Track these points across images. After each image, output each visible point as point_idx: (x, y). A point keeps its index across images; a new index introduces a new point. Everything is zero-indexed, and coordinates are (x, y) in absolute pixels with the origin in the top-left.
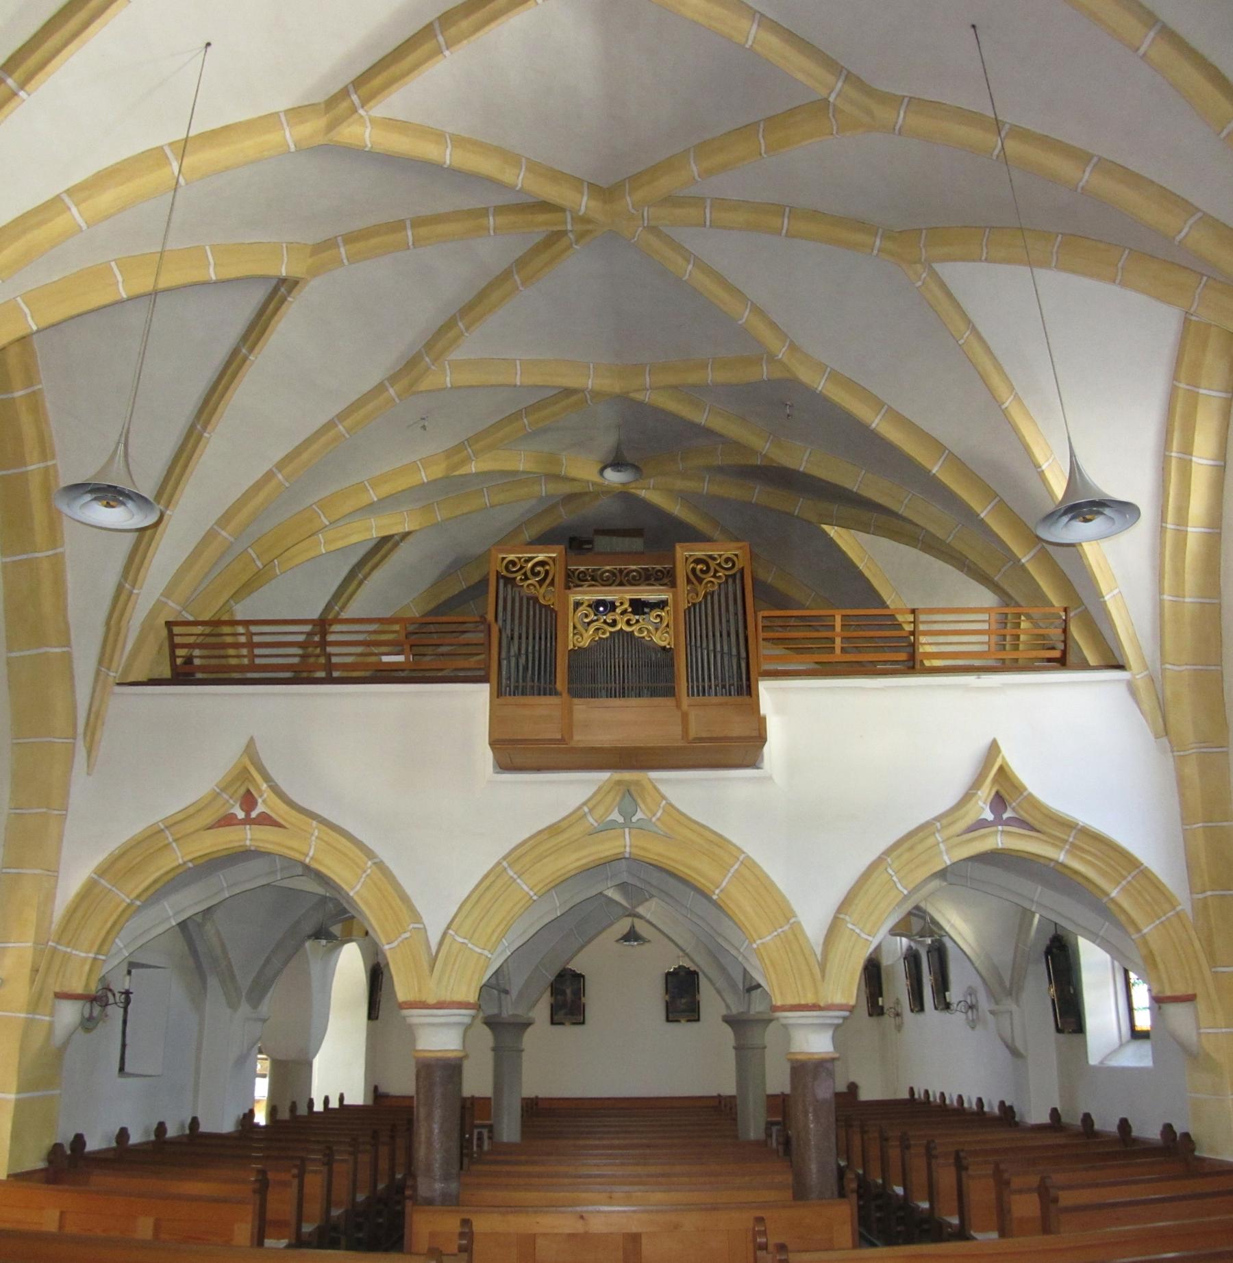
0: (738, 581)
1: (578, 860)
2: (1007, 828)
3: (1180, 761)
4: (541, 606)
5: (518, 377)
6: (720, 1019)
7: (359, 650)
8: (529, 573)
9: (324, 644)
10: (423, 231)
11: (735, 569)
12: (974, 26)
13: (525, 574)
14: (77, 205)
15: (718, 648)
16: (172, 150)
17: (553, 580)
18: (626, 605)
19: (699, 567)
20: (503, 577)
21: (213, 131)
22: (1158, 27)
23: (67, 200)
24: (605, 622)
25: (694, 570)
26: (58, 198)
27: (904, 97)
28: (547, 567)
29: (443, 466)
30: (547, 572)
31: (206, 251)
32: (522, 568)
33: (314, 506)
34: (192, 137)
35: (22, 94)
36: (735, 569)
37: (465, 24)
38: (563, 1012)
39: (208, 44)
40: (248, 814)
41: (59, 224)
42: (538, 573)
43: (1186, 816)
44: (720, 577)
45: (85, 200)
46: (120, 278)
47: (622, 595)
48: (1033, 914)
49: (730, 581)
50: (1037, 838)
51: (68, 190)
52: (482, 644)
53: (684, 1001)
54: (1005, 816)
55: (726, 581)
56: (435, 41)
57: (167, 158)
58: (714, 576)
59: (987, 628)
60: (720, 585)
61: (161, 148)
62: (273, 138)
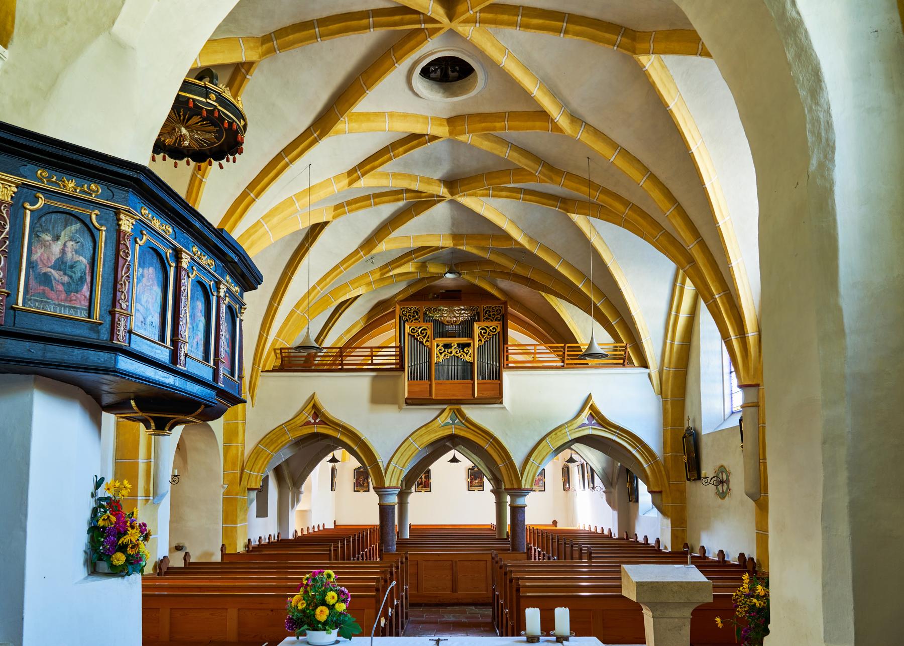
0: (497, 336)
1: (435, 436)
2: (593, 427)
3: (665, 403)
4: (425, 346)
5: (412, 244)
7: (353, 354)
8: (420, 333)
9: (341, 356)
10: (376, 200)
11: (496, 332)
12: (588, 158)
13: (418, 333)
14: (266, 224)
15: (489, 362)
17: (429, 336)
18: (456, 345)
19: (483, 331)
20: (410, 335)
24: (448, 352)
25: (481, 332)
27: (565, 172)
28: (426, 331)
29: (379, 274)
30: (426, 333)
32: (417, 331)
33: (328, 294)
35: (257, 200)
36: (496, 332)
37: (401, 149)
38: (421, 486)
40: (315, 421)
41: (261, 231)
42: (423, 333)
43: (665, 424)
44: (490, 335)
45: (269, 221)
46: (271, 235)
47: (454, 341)
49: (494, 336)
50: (605, 431)
53: (477, 481)
54: (593, 422)
55: (493, 336)
56: (368, 20)
58: (488, 335)
59: (372, 518)
60: (490, 338)
62: (330, 190)
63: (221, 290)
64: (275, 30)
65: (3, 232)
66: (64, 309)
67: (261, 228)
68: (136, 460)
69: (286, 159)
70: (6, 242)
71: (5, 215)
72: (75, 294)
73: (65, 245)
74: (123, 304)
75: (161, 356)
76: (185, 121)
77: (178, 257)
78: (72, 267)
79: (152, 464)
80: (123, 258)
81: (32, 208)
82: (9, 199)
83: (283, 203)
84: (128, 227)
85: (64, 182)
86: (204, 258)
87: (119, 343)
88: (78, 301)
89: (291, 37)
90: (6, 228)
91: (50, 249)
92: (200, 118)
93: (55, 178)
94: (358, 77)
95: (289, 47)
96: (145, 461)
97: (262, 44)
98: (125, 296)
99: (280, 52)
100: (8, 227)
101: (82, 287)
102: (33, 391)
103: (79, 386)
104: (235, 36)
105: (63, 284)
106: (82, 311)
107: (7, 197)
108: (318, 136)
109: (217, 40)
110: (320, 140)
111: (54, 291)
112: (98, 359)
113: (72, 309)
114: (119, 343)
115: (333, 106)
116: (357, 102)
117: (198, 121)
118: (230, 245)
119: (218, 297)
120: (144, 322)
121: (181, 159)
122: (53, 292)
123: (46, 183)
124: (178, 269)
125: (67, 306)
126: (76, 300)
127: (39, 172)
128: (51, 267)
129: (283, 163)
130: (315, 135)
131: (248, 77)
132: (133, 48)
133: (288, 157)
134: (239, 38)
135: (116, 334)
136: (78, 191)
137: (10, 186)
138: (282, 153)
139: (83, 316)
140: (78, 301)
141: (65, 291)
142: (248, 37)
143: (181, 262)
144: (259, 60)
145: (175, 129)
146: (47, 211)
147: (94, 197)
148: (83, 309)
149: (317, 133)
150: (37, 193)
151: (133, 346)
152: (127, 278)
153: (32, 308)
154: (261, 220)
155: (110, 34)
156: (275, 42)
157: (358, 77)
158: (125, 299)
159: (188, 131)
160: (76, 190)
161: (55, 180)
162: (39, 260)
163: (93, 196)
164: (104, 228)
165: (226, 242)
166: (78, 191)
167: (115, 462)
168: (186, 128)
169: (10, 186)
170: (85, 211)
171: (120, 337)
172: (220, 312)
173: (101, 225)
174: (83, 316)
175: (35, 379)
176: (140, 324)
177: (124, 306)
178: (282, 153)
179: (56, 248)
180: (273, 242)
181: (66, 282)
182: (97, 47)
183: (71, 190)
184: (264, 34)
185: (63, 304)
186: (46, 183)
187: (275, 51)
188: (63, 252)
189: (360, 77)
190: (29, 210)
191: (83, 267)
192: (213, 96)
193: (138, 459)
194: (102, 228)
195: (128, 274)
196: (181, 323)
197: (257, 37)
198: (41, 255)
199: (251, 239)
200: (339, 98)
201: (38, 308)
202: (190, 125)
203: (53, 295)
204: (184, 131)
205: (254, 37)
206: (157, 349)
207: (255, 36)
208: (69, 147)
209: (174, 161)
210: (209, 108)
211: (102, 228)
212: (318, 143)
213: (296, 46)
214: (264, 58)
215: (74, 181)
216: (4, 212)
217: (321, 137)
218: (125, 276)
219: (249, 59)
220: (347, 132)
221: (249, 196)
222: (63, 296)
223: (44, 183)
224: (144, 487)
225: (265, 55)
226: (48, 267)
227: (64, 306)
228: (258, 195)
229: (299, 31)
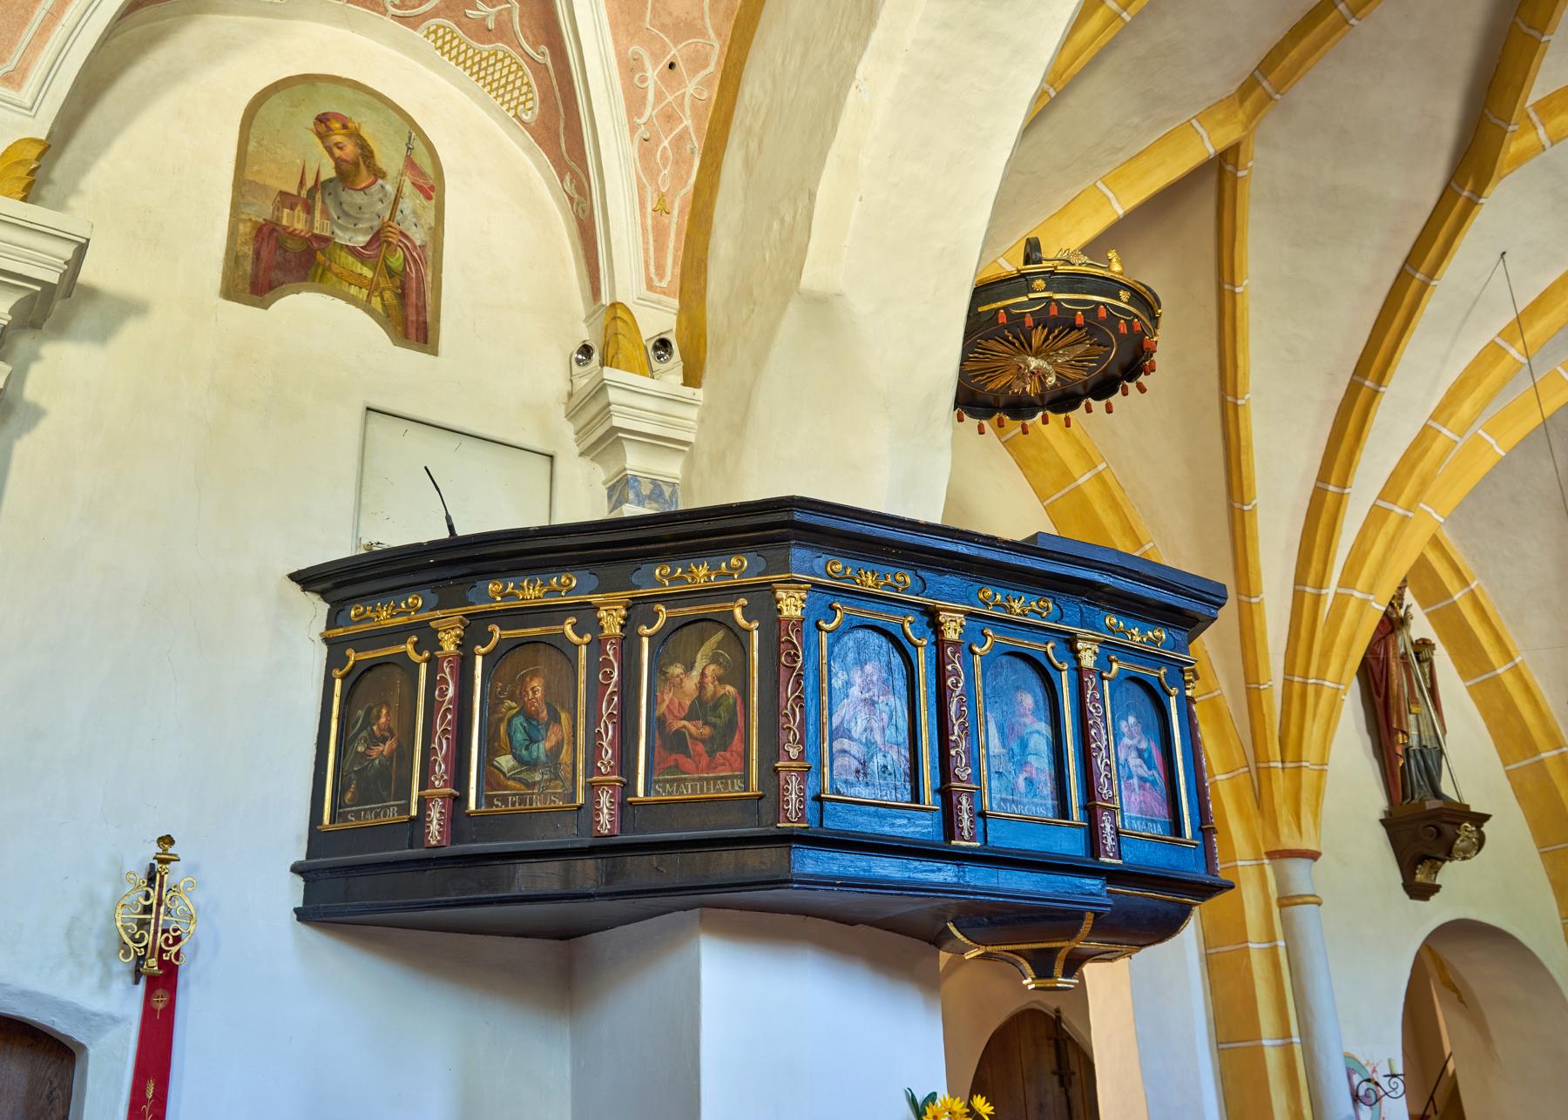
6: (242, 314)
14: (1444, 426)
16: (1503, 339)
21: (1533, 304)
22: (1272, 944)
23: (1434, 425)
26: (1426, 427)
31: (1558, 372)
34: (1550, 417)
35: (1382, 389)
39: (1504, 253)
41: (1437, 447)
45: (1449, 419)
46: (1493, 442)
48: (731, 613)
51: (1431, 416)
52: (821, 825)
57: (1503, 349)
61: (1493, 341)
63: (1082, 654)
64: (1258, 63)
65: (609, 684)
66: (707, 785)
67: (1434, 439)
68: (1256, 1042)
69: (1418, 276)
70: (613, 699)
71: (612, 658)
72: (722, 753)
73: (703, 675)
74: (791, 750)
75: (912, 829)
76: (1026, 345)
77: (931, 617)
78: (715, 707)
79: (1298, 1049)
80: (786, 666)
81: (649, 631)
82: (618, 631)
83: (1478, 361)
84: (794, 608)
85: (691, 572)
86: (1016, 606)
87: (789, 825)
88: (727, 764)
89: (1294, 54)
90: (612, 678)
91: (682, 687)
92: (1044, 328)
93: (680, 570)
94: (1514, 23)
95: (1295, 74)
96: (1279, 1042)
97: (1242, 101)
98: (795, 734)
99: (1282, 94)
100: (616, 674)
101: (732, 738)
102: (699, 942)
103: (803, 914)
104: (1178, 124)
105: (703, 741)
106: (735, 781)
107: (615, 628)
108: (1472, 192)
109: (1144, 150)
110: (1480, 197)
111: (690, 757)
112: (761, 862)
113: (719, 782)
114: (789, 825)
115: (1483, 112)
116: (1531, 74)
117: (1043, 336)
118: (1068, 558)
119: (1079, 671)
120: (863, 770)
121: (1075, 406)
122: (689, 760)
123: (667, 584)
124: (940, 644)
125: (712, 778)
126: (724, 764)
127: (657, 572)
128: (684, 719)
129: (1414, 285)
130: (1466, 193)
131: (1240, 174)
132: (838, 295)
133: (1421, 270)
134: (1189, 121)
135: (784, 809)
136: (712, 578)
137: (616, 610)
138: (1407, 267)
139: (737, 788)
140: (727, 764)
141: (707, 752)
142: (1209, 108)
143: (942, 632)
144: (1245, 133)
145: (1021, 367)
146: (677, 627)
147: (669, 586)
148: (736, 777)
149: (1469, 186)
150: (654, 607)
151: (827, 823)
152: (798, 700)
153: (662, 796)
154: (1430, 423)
155: (799, 293)
156: (1265, 84)
157: (1514, 23)
158: (794, 741)
159: (1042, 358)
160: (709, 577)
161: (681, 573)
162: (666, 713)
163: (736, 576)
164: (755, 625)
165: (1055, 555)
166: (712, 578)
167: (1218, 1050)
168: (1036, 355)
169: (616, 610)
170: (724, 607)
171: (791, 813)
172: (1085, 700)
173: (749, 621)
174: (737, 788)
175: (701, 916)
176: (852, 778)
177: (794, 753)
178: (1407, 267)
179: (691, 683)
180: (1503, 454)
181: (707, 737)
182: (791, 321)
183: (702, 581)
184: (1239, 84)
185: (706, 775)
186: (667, 584)
187: (1271, 98)
188: (701, 686)
189: (1518, 19)
190: (646, 636)
191: (731, 701)
192: (1040, 283)
193: (1261, 1039)
194: (752, 626)
195: (797, 694)
196: (953, 752)
197: (1229, 97)
198: (670, 702)
199: (1417, 472)
200: (1489, 89)
201: (670, 794)
202: (1038, 348)
203: (688, 763)
204: (1034, 363)
205: (1221, 101)
206: (896, 817)
207: (1224, 97)
208: (679, 517)
209: (1020, 422)
210: (1038, 308)
211: (752, 626)
212: (1477, 208)
213: (1308, 64)
214: (1253, 124)
215: (706, 565)
216: (611, 653)
217: (1478, 192)
218: (793, 697)
219: (1222, 145)
220: (1547, 144)
221: (1364, 389)
222: (704, 761)
223: (665, 585)
224: (1289, 1107)
225: (1255, 116)
226: (681, 719)
227: (707, 779)
228: (1380, 381)
229: (1306, 33)
